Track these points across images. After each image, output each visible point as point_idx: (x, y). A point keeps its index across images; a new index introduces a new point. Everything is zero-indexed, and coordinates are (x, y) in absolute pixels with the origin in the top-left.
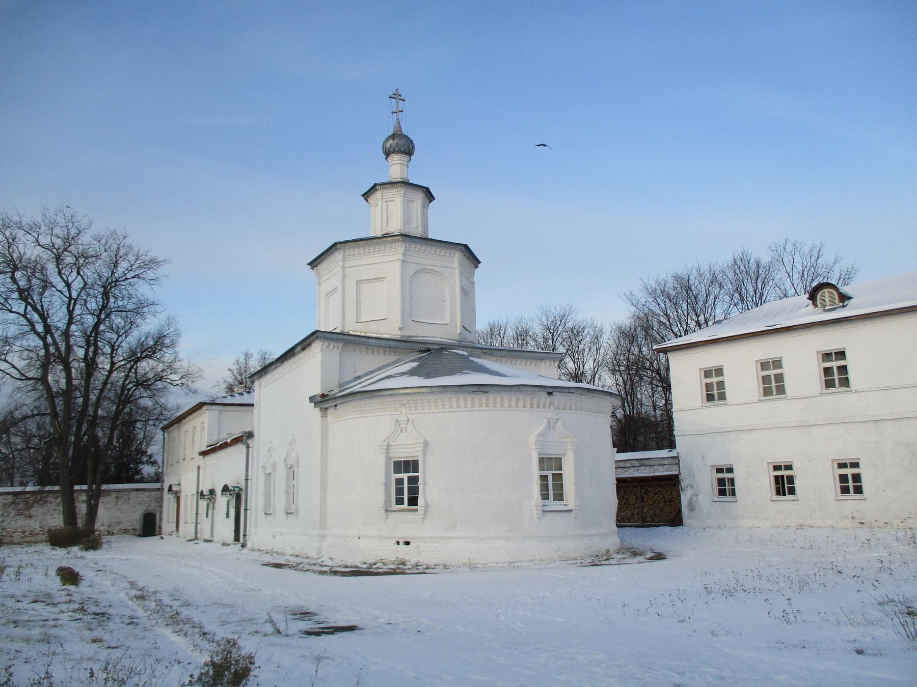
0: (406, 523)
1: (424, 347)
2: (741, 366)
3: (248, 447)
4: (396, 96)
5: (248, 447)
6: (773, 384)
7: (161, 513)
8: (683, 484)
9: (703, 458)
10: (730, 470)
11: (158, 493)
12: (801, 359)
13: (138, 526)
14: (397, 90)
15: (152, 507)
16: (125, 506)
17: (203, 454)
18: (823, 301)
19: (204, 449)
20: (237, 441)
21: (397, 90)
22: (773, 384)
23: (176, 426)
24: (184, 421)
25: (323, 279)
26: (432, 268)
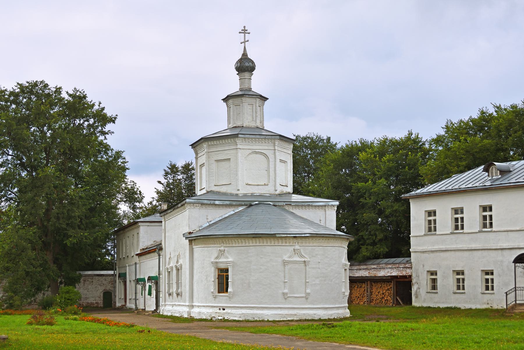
0: (223, 300)
1: (248, 203)
2: (443, 209)
3: (159, 255)
4: (244, 31)
5: (159, 255)
6: (458, 224)
7: (115, 292)
8: (414, 281)
9: (423, 266)
10: (463, 274)
11: (112, 278)
12: (472, 207)
13: (100, 302)
14: (244, 27)
15: (109, 287)
16: (90, 287)
17: (139, 255)
18: (492, 173)
19: (139, 252)
20: (153, 251)
21: (244, 27)
22: (458, 224)
23: (122, 232)
24: (126, 230)
25: (199, 155)
26: (260, 151)
